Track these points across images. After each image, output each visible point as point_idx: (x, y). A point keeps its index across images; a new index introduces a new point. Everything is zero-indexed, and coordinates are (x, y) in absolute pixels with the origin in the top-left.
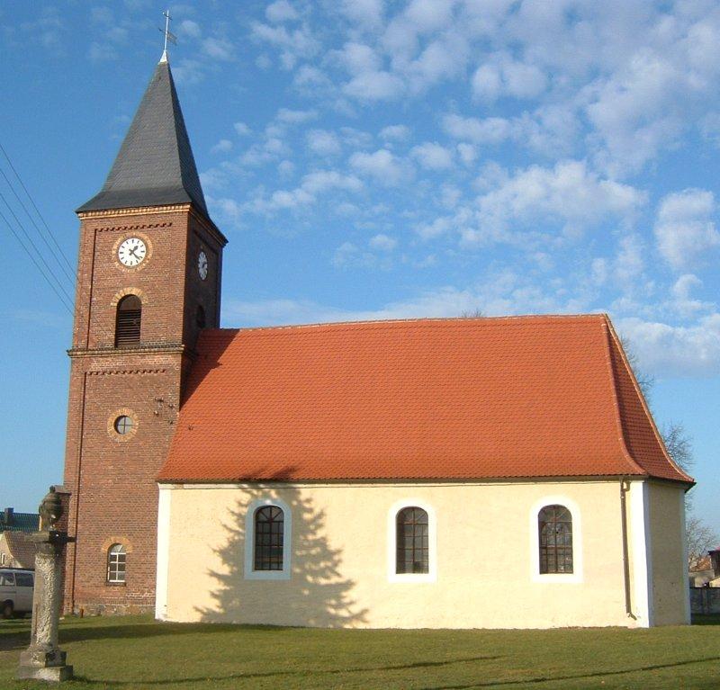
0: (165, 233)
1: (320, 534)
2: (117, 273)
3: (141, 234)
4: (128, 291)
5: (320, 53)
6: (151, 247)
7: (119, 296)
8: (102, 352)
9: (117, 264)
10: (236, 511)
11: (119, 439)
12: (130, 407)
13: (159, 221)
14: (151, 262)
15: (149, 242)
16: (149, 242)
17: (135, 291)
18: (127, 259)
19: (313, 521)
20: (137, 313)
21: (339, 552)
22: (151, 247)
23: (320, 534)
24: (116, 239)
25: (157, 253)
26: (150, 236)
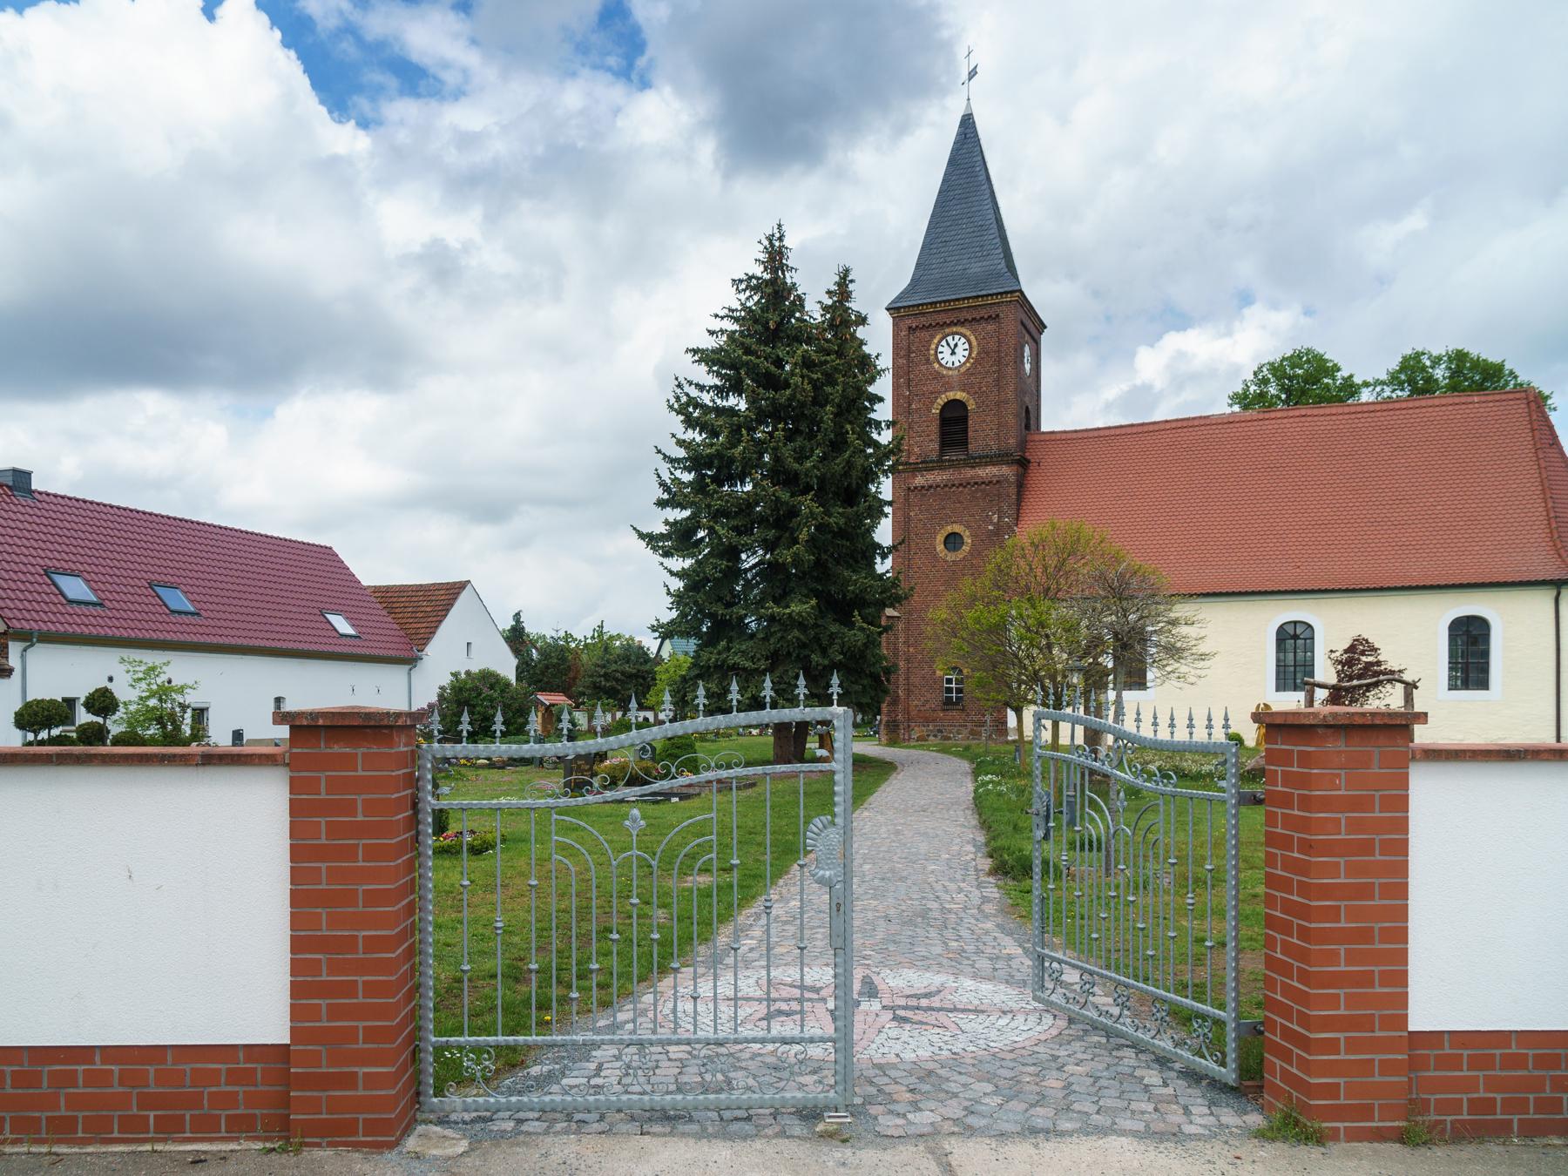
0: (990, 327)
1: (758, 270)
2: (938, 376)
3: (963, 330)
4: (951, 395)
5: (1264, 327)
6: (975, 343)
7: (942, 400)
8: (925, 465)
9: (936, 366)
10: (681, 436)
11: (960, 555)
12: (961, 523)
13: (984, 313)
14: (976, 360)
15: (972, 338)
16: (972, 338)
17: (960, 395)
18: (945, 356)
19: (756, 289)
20: (964, 420)
21: (455, 675)
22: (975, 343)
23: (758, 270)
24: (933, 337)
25: (984, 352)
26: (974, 332)
